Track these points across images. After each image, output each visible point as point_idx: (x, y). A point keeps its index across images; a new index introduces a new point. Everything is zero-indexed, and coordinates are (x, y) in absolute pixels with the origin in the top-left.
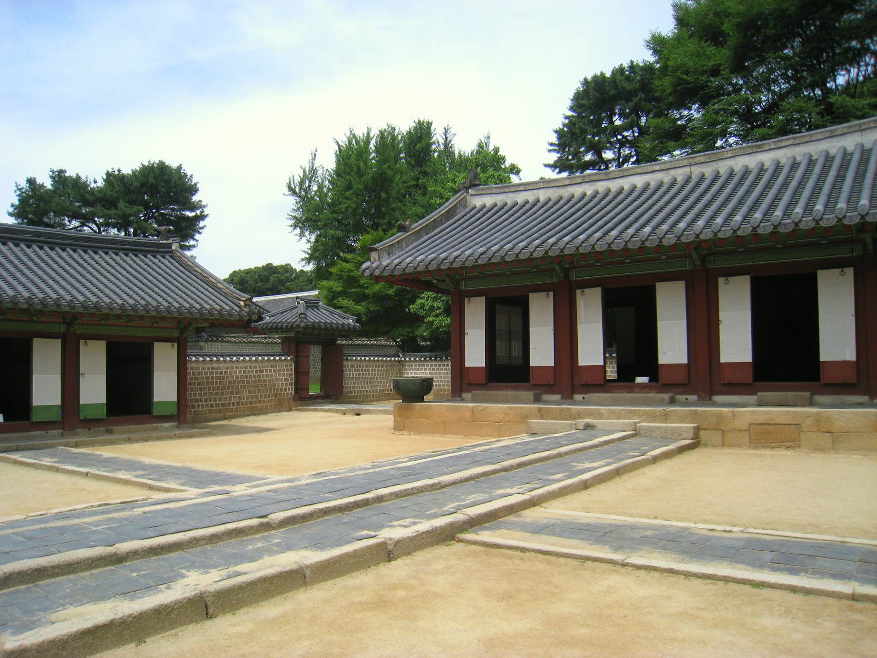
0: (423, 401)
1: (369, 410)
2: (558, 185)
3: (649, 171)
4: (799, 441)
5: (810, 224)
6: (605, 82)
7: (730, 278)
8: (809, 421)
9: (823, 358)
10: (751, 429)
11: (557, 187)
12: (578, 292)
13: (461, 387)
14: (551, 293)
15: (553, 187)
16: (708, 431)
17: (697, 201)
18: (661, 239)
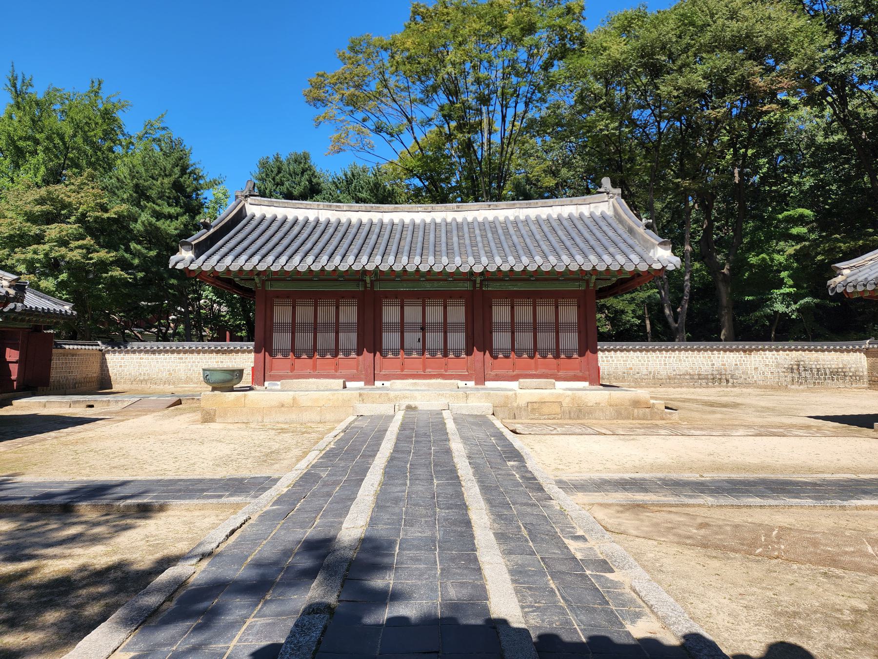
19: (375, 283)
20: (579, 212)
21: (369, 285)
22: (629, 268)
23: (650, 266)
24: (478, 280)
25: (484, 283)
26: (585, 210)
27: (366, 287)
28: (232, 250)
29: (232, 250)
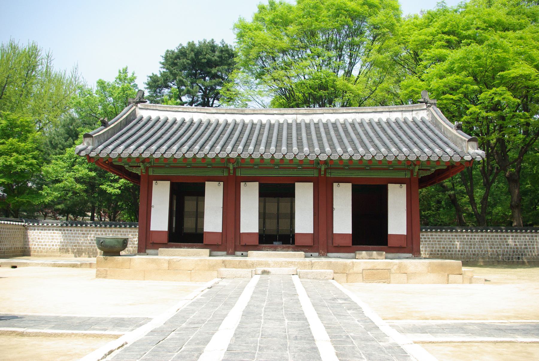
0: (120, 255)
1: (26, 263)
2: (208, 112)
3: (271, 113)
4: (390, 279)
5: (324, 157)
6: (214, 51)
7: (158, 182)
8: (395, 267)
9: (390, 232)
10: (364, 272)
11: (207, 113)
12: (154, 182)
13: (146, 245)
14: (222, 183)
15: (204, 113)
16: (338, 274)
17: (420, 138)
18: (317, 156)
19: (237, 170)
20: (404, 117)
21: (232, 172)
22: (446, 159)
23: (462, 158)
24: (323, 168)
25: (328, 171)
26: (409, 116)
27: (229, 173)
28: (123, 142)
29: (123, 142)
